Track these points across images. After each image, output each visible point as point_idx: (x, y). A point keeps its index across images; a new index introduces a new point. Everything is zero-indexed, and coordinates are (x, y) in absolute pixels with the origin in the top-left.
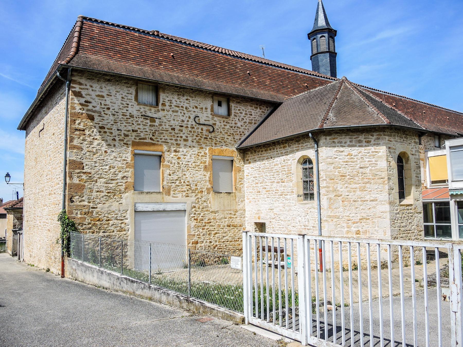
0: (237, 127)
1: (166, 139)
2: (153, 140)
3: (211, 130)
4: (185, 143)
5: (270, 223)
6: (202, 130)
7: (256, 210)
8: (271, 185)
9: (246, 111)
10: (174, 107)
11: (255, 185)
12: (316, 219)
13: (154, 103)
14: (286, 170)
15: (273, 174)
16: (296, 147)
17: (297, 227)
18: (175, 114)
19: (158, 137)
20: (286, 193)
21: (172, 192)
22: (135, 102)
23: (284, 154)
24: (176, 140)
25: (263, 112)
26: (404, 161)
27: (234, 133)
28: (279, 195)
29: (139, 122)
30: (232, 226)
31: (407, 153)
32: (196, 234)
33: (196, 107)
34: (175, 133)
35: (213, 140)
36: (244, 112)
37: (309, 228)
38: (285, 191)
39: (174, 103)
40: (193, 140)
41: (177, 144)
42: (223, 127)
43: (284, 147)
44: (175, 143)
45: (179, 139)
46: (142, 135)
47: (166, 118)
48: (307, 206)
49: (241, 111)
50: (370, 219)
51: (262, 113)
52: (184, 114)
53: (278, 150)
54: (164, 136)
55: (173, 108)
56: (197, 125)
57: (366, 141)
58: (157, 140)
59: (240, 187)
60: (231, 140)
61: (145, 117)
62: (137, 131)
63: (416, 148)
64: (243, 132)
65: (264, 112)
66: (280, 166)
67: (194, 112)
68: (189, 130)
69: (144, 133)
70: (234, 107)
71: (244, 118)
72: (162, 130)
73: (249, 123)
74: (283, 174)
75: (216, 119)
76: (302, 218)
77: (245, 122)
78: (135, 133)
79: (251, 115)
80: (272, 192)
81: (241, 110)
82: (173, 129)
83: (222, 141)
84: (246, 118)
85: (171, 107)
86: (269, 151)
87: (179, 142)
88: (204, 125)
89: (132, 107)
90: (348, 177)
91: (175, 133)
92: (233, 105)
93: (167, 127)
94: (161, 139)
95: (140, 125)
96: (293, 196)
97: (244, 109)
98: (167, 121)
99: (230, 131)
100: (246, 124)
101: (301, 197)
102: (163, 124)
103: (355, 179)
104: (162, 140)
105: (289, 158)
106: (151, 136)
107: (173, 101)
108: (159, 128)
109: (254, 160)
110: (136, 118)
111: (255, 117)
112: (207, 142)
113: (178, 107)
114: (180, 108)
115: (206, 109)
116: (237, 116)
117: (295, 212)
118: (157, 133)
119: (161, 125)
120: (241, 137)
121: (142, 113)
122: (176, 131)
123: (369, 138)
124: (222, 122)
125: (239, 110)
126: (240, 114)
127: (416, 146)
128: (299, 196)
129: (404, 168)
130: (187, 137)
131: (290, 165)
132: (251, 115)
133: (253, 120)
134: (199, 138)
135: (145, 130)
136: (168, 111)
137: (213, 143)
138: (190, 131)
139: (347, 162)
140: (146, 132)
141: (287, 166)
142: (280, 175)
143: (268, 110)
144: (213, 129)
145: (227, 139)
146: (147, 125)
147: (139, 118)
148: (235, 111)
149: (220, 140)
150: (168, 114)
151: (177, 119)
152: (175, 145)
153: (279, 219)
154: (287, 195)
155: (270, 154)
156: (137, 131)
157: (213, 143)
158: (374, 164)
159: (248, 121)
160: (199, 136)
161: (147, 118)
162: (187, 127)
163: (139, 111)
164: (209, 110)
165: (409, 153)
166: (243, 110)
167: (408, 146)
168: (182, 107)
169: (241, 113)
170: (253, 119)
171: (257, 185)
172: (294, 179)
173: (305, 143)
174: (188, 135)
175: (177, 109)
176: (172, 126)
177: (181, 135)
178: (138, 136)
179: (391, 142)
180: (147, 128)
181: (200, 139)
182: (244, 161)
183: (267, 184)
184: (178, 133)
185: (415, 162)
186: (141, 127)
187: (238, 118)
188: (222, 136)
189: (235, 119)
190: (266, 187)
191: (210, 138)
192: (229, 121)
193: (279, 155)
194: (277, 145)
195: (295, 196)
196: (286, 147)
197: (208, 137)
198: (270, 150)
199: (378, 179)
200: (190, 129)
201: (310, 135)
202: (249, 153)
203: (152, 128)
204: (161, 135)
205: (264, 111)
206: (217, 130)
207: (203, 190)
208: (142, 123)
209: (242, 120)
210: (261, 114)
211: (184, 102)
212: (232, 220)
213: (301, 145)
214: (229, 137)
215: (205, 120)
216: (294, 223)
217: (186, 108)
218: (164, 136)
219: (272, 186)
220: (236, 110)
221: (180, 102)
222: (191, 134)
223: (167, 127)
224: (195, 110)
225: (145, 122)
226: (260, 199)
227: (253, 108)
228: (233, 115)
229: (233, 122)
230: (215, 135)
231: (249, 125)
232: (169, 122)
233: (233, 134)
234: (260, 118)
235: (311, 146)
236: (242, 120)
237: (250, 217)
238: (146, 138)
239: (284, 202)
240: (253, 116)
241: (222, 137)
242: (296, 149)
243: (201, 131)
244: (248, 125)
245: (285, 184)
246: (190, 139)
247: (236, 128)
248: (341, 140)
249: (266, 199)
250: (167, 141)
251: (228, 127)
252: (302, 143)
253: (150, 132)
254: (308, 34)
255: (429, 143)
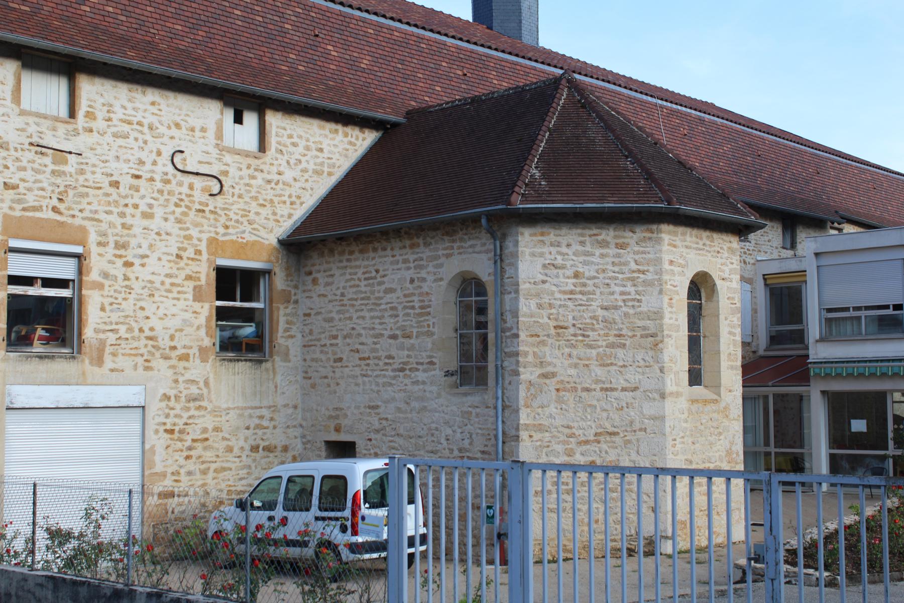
0: (284, 183)
1: (96, 212)
2: (60, 213)
3: (216, 190)
4: (146, 223)
5: (368, 442)
6: (191, 187)
7: (331, 408)
8: (375, 343)
9: (308, 140)
10: (119, 123)
12: (492, 434)
13: (64, 112)
14: (417, 305)
17: (439, 454)
18: (120, 142)
19: (74, 206)
20: (415, 366)
21: (108, 358)
22: (13, 106)
23: (412, 265)
24: (122, 215)
25: (350, 143)
26: (703, 295)
27: (273, 198)
28: (394, 370)
29: (24, 163)
31: (710, 276)
32: (170, 470)
33: (178, 126)
34: (119, 195)
35: (221, 216)
36: (302, 143)
37: (470, 455)
38: (411, 360)
39: (119, 114)
40: (166, 216)
41: (124, 226)
42: (247, 181)
43: (412, 246)
44: (119, 221)
45: (129, 210)
46: (31, 199)
47: (97, 152)
48: (470, 400)
49: (295, 140)
51: (348, 147)
52: (145, 142)
54: (89, 204)
55: (115, 126)
56: (179, 174)
57: (617, 244)
58: (72, 212)
59: (287, 347)
60: (266, 218)
61: (39, 149)
62: (17, 187)
63: (732, 263)
64: (299, 197)
65: (355, 145)
66: (399, 293)
67: (172, 138)
68: (156, 189)
69: (36, 192)
71: (303, 159)
72: (84, 186)
73: (316, 172)
74: (408, 315)
75: (228, 158)
76: (454, 431)
77: (305, 171)
78: (11, 191)
79: (321, 150)
80: (376, 361)
82: (116, 184)
83: (244, 220)
85: (110, 123)
87: (129, 220)
88: (197, 174)
89: (6, 118)
91: (119, 195)
92: (274, 119)
93: (98, 177)
94: (81, 211)
95: (24, 169)
96: (433, 373)
98: (97, 163)
99: (263, 192)
100: (306, 176)
101: (454, 378)
102: (88, 169)
103: (588, 336)
104: (84, 215)
105: (424, 275)
106: (55, 202)
107: (117, 108)
108: (77, 180)
109: (327, 273)
110: (16, 150)
111: (330, 156)
112: (204, 221)
113: (130, 123)
114: (135, 126)
115: (203, 130)
116: (285, 152)
117: (437, 414)
118: (71, 193)
119: (82, 172)
120: (292, 211)
121: (31, 136)
122: (123, 190)
123: (624, 237)
125: (290, 136)
126: (291, 149)
127: (732, 259)
129: (704, 312)
130: (151, 206)
131: (427, 293)
132: (321, 150)
133: (326, 165)
134: (184, 209)
135: (40, 185)
136: (102, 134)
137: (218, 224)
138: (161, 192)
139: (572, 292)
140: (43, 189)
141: (421, 294)
142: (400, 319)
143: (364, 139)
144: (219, 185)
145: (257, 214)
146: (44, 172)
147: (22, 150)
148: (279, 139)
149: (239, 217)
150: (101, 142)
151: (125, 157)
152: (120, 227)
153: (393, 433)
154: (417, 370)
155: (374, 262)
156: (15, 187)
157: (218, 224)
158: (633, 300)
159: (311, 167)
160: (182, 204)
161: (44, 150)
162: (152, 179)
163: (23, 130)
164: (211, 134)
165: (715, 275)
166: (300, 137)
167: (714, 259)
168: (140, 124)
169: (295, 145)
171: (334, 341)
172: (436, 330)
173: (470, 239)
174: (153, 202)
175: (126, 128)
176: (112, 175)
177: (136, 200)
178: (19, 201)
179: (674, 249)
180: (46, 180)
181: (185, 214)
182: (299, 276)
183: (363, 339)
184: (126, 197)
185: (728, 298)
186: (29, 175)
187: (286, 157)
188: (242, 206)
189: (280, 161)
190: (360, 347)
191: (211, 212)
192: (262, 167)
193: (399, 266)
194: (392, 240)
195: (438, 373)
196: (418, 245)
200: (159, 185)
201: (484, 221)
203: (59, 181)
204: (82, 200)
205: (353, 140)
206: (231, 190)
207: (191, 352)
208: (31, 164)
209: (296, 164)
210: (347, 150)
211: (145, 110)
212: (265, 434)
213: (458, 244)
214: (260, 210)
215: (200, 162)
216: (433, 444)
217: (151, 128)
218: (89, 204)
219: (378, 346)
221: (134, 109)
222: (162, 199)
223: (98, 177)
224: (174, 132)
225: (39, 161)
226: (342, 377)
227: (327, 132)
229: (274, 169)
231: (315, 178)
232: (103, 165)
233: (272, 201)
234: (342, 159)
236: (296, 164)
238: (41, 207)
239: (409, 387)
241: (244, 210)
242: (445, 252)
243: (189, 192)
244: (313, 179)
245: (412, 341)
246: (159, 212)
247: (281, 185)
248: (559, 239)
249: (360, 380)
250: (96, 216)
251: (259, 181)
252: (461, 240)
253: (53, 191)
255: (766, 238)
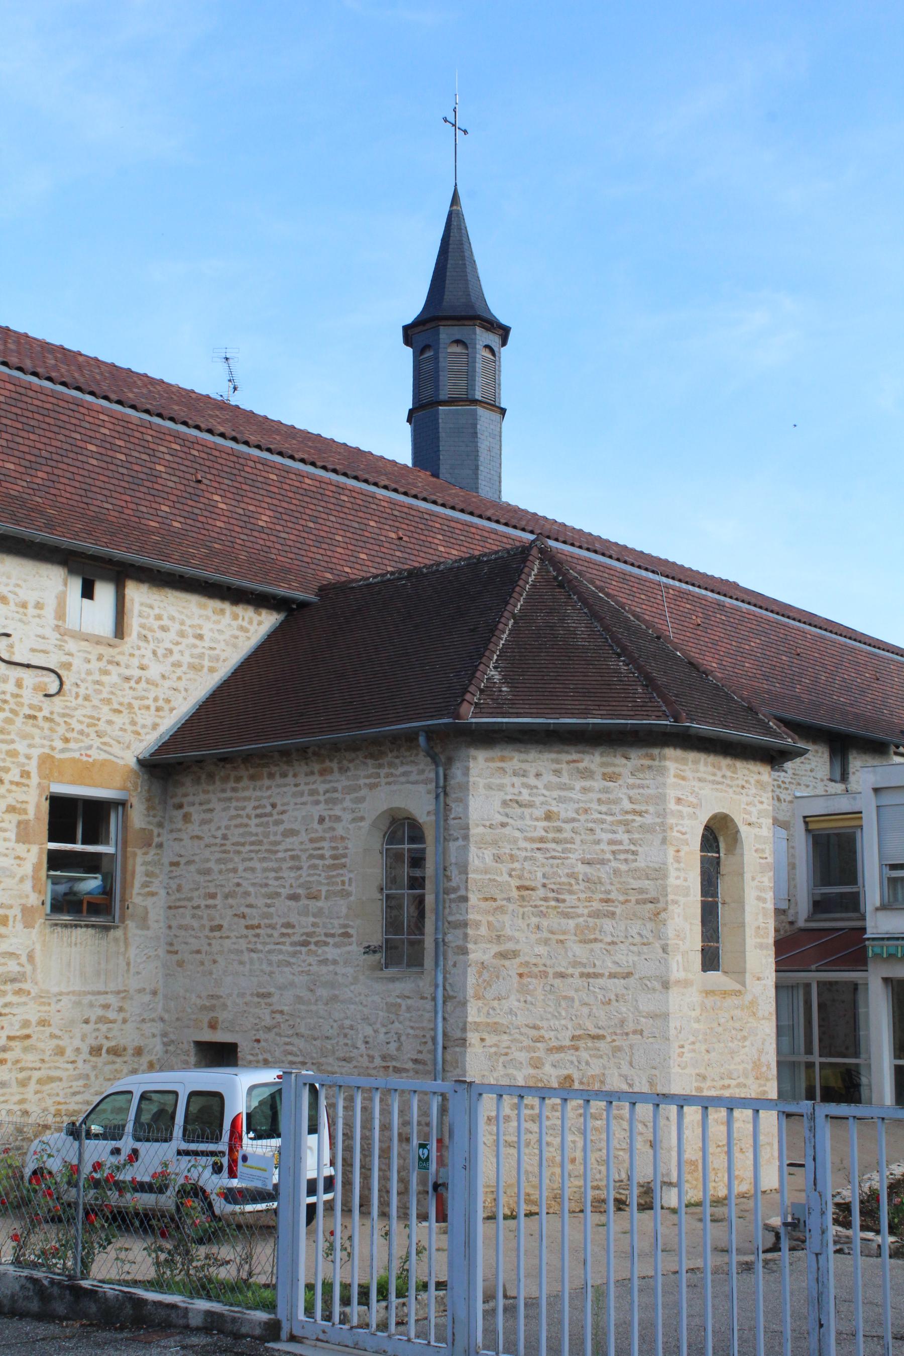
3: (53, 688)
5: (256, 1044)
6: (19, 684)
9: (182, 623)
11: (203, 903)
12: (428, 1036)
14: (328, 854)
15: (273, 865)
16: (368, 777)
17: (354, 1063)
23: (322, 798)
25: (241, 628)
26: (722, 846)
28: (293, 944)
30: (108, 1052)
31: (732, 820)
35: (59, 724)
36: (175, 627)
37: (398, 1065)
38: (317, 930)
42: (96, 677)
49: (165, 622)
50: (609, 1039)
53: (301, 779)
57: (604, 774)
64: (168, 701)
70: (142, 604)
71: (176, 649)
73: (193, 667)
74: (314, 867)
75: (71, 645)
76: (376, 1031)
79: (200, 637)
80: (269, 931)
81: (165, 617)
83: (91, 731)
84: (179, 647)
86: (267, 782)
88: (28, 666)
90: (541, 892)
96: (348, 948)
97: (176, 615)
99: (119, 693)
100: (179, 672)
103: (564, 901)
105: (339, 813)
109: (205, 807)
111: (213, 645)
112: (36, 731)
115: (39, 606)
116: (150, 638)
117: (352, 1007)
120: (158, 720)
123: (615, 765)
124: (93, 657)
125: (159, 617)
126: (159, 634)
128: (369, 950)
129: (723, 869)
131: (342, 838)
132: (200, 637)
133: (206, 658)
137: (55, 736)
141: (333, 839)
142: (304, 873)
143: (260, 623)
144: (57, 683)
145: (110, 722)
148: (143, 621)
149: (83, 727)
153: (290, 1032)
154: (326, 944)
155: (269, 793)
157: (55, 736)
159: (186, 659)
160: (6, 707)
164: (49, 612)
165: (738, 819)
166: (172, 618)
169: (164, 629)
170: (207, 652)
171: (211, 902)
173: (402, 763)
182: (165, 809)
183: (251, 900)
185: (756, 851)
187: (152, 646)
189: (143, 652)
190: (247, 911)
191: (46, 719)
192: (118, 658)
193: (304, 799)
195: (355, 949)
197: (40, 715)
198: (271, 776)
199: (638, 902)
201: (422, 740)
202: (188, 781)
205: (245, 624)
206: (75, 689)
209: (165, 656)
210: (237, 637)
214: (115, 718)
215: (33, 650)
219: (272, 910)
220: (148, 617)
227: (209, 612)
228: (134, 634)
229: (135, 662)
230: (67, 707)
231: (192, 674)
233: (130, 706)
235: (422, 777)
236: (165, 656)
237: (178, 1019)
239: (315, 968)
240: (207, 644)
241: (92, 717)
242: (367, 781)
243: (16, 690)
244: (188, 676)
247: (143, 684)
248: (525, 766)
249: (246, 957)
251: (114, 678)
252: (391, 765)
254: (406, 329)
255: (808, 767)
